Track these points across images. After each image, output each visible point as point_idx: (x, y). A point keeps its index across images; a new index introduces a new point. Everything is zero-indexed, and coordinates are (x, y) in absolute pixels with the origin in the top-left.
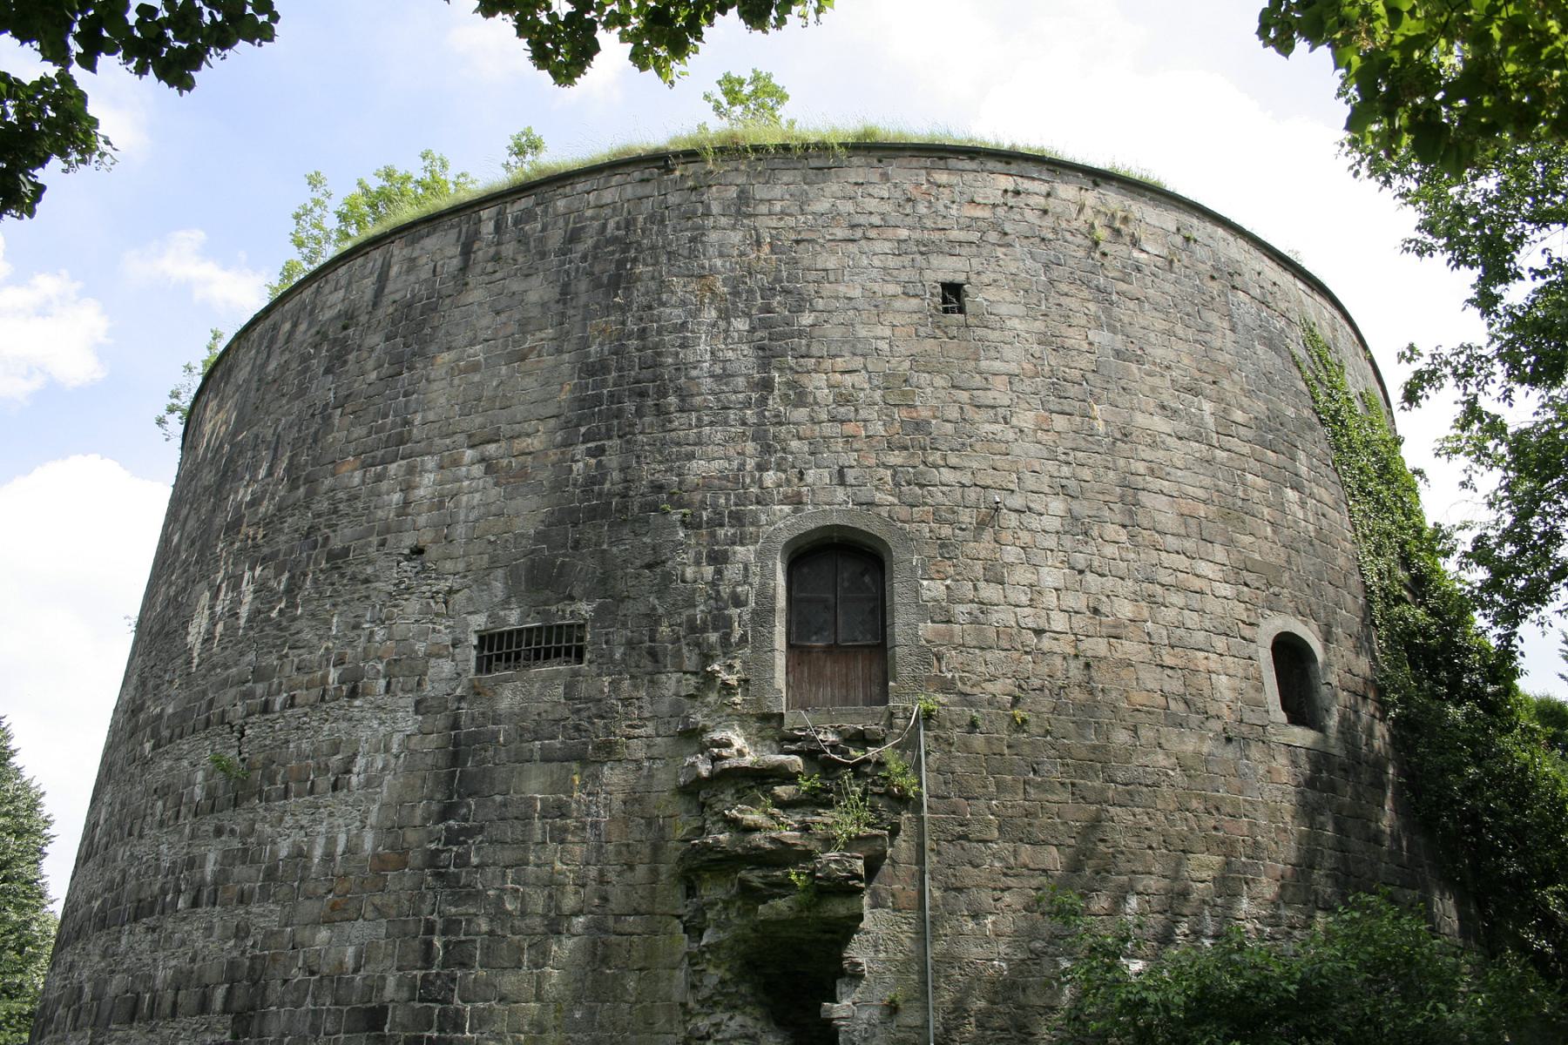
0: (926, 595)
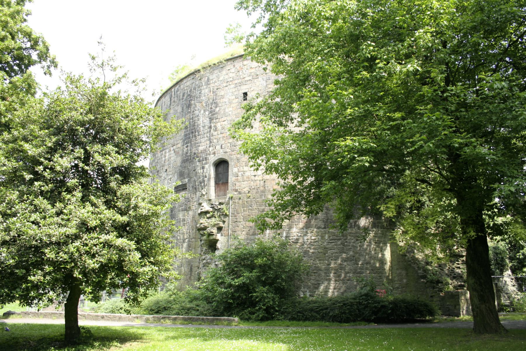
0: (234, 171)
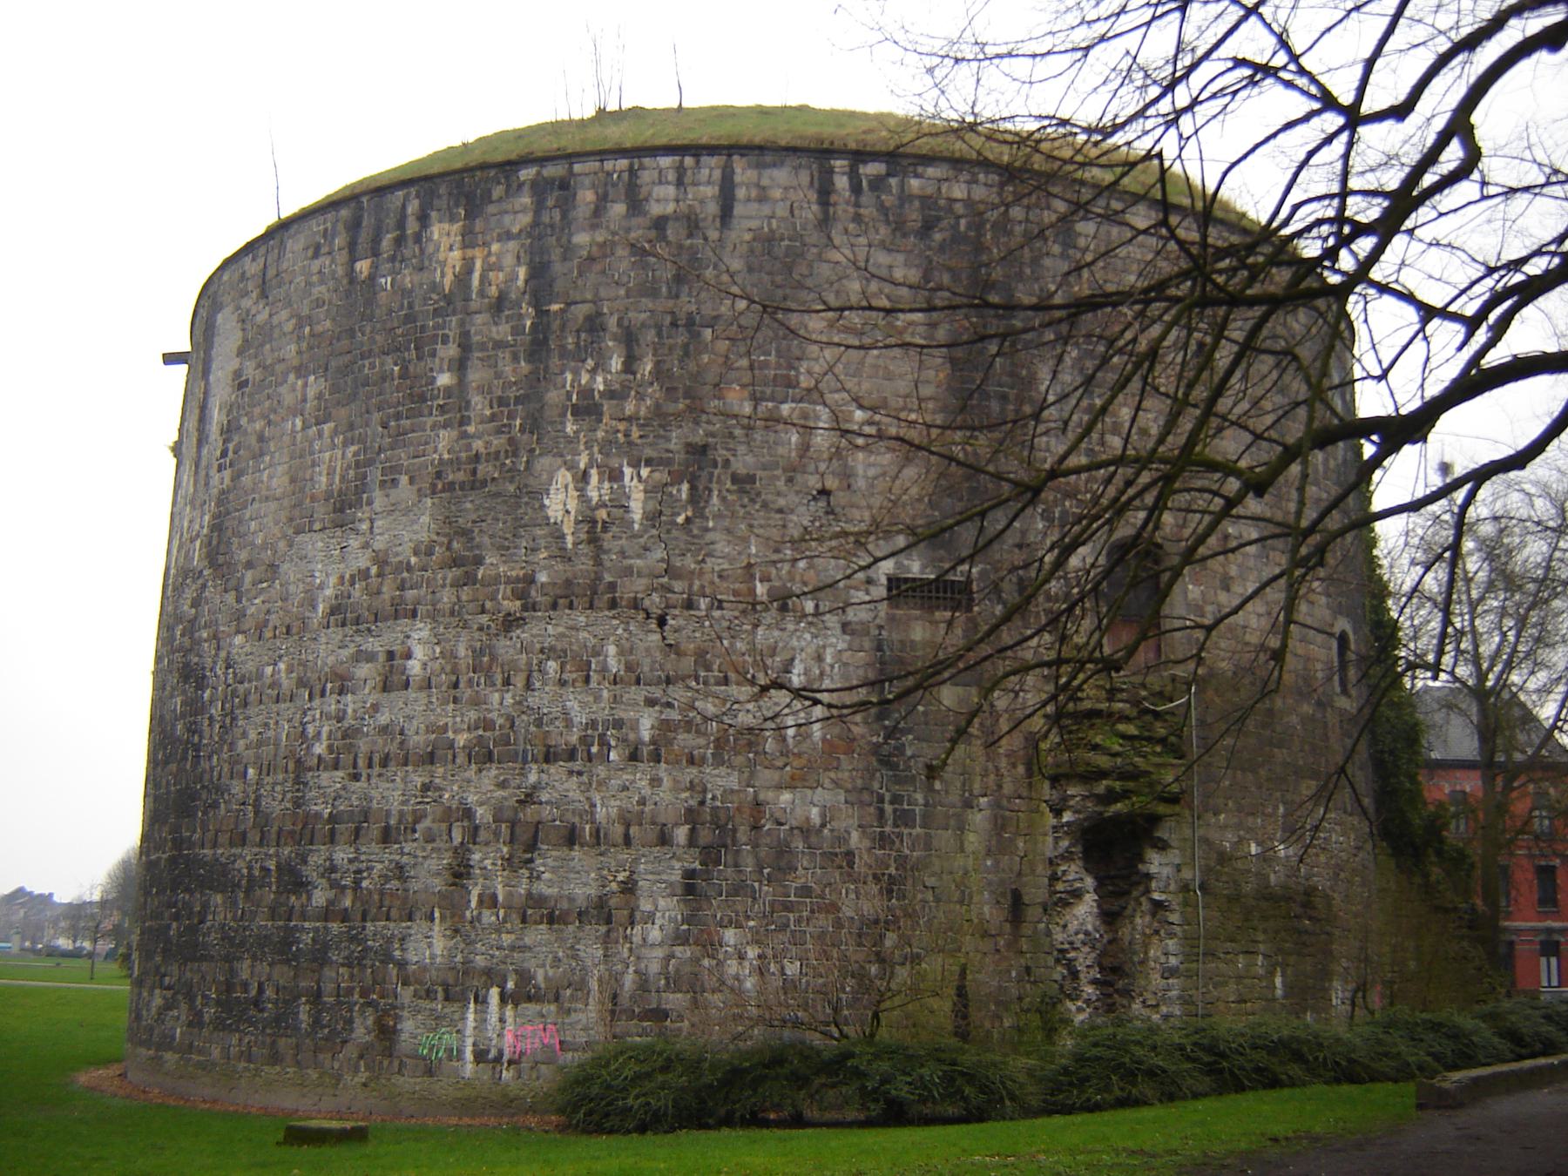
0: (1190, 596)
